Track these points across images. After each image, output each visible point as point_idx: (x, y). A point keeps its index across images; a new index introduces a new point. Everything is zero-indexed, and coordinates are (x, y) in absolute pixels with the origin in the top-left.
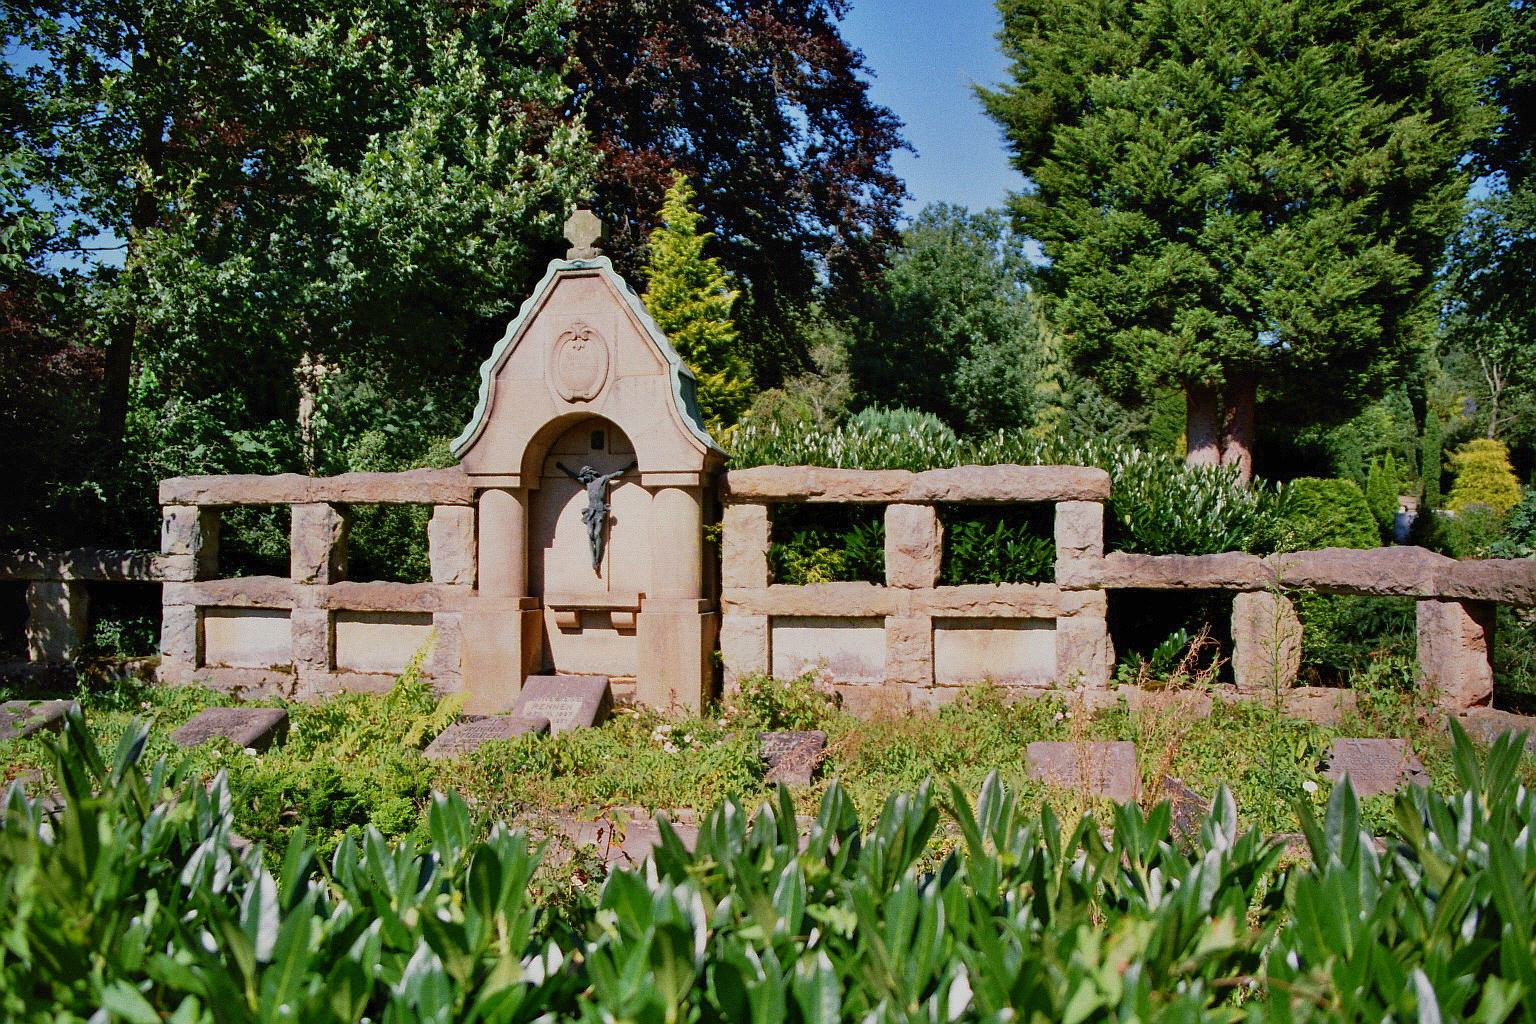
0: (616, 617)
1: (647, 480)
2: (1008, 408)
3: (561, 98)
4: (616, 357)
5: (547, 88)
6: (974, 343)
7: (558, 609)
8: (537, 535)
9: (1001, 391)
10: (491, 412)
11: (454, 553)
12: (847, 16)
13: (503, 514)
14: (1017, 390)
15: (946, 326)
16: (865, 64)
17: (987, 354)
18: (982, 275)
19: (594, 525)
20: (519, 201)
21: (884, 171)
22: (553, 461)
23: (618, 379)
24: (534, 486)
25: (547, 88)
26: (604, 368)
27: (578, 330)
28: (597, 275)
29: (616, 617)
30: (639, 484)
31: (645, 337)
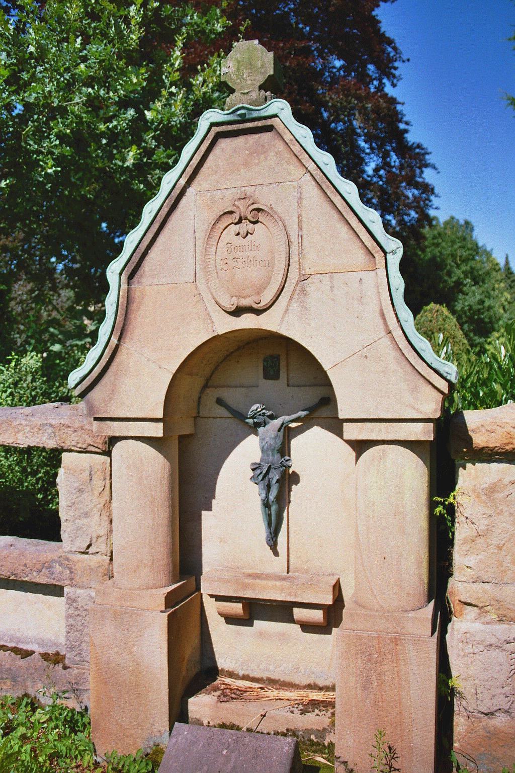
0: (298, 613)
1: (352, 432)
2: (485, 323)
3: (220, 30)
4: (301, 245)
5: (208, 22)
6: (465, 285)
7: (219, 598)
8: (190, 495)
9: (482, 314)
10: (122, 331)
11: (86, 515)
12: (399, 84)
13: (142, 470)
14: (491, 313)
15: (450, 276)
16: (405, 119)
17: (474, 292)
18: (470, 246)
19: (269, 487)
20: (177, 108)
21: (420, 180)
22: (211, 395)
23: (304, 278)
24: (187, 430)
25: (208, 22)
26: (284, 262)
27: (243, 208)
28: (270, 128)
29: (298, 613)
30: (340, 434)
31: (343, 213)
